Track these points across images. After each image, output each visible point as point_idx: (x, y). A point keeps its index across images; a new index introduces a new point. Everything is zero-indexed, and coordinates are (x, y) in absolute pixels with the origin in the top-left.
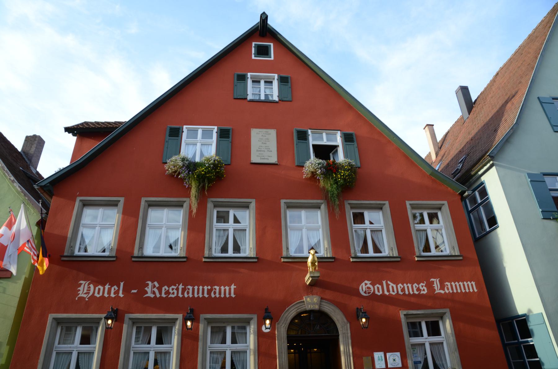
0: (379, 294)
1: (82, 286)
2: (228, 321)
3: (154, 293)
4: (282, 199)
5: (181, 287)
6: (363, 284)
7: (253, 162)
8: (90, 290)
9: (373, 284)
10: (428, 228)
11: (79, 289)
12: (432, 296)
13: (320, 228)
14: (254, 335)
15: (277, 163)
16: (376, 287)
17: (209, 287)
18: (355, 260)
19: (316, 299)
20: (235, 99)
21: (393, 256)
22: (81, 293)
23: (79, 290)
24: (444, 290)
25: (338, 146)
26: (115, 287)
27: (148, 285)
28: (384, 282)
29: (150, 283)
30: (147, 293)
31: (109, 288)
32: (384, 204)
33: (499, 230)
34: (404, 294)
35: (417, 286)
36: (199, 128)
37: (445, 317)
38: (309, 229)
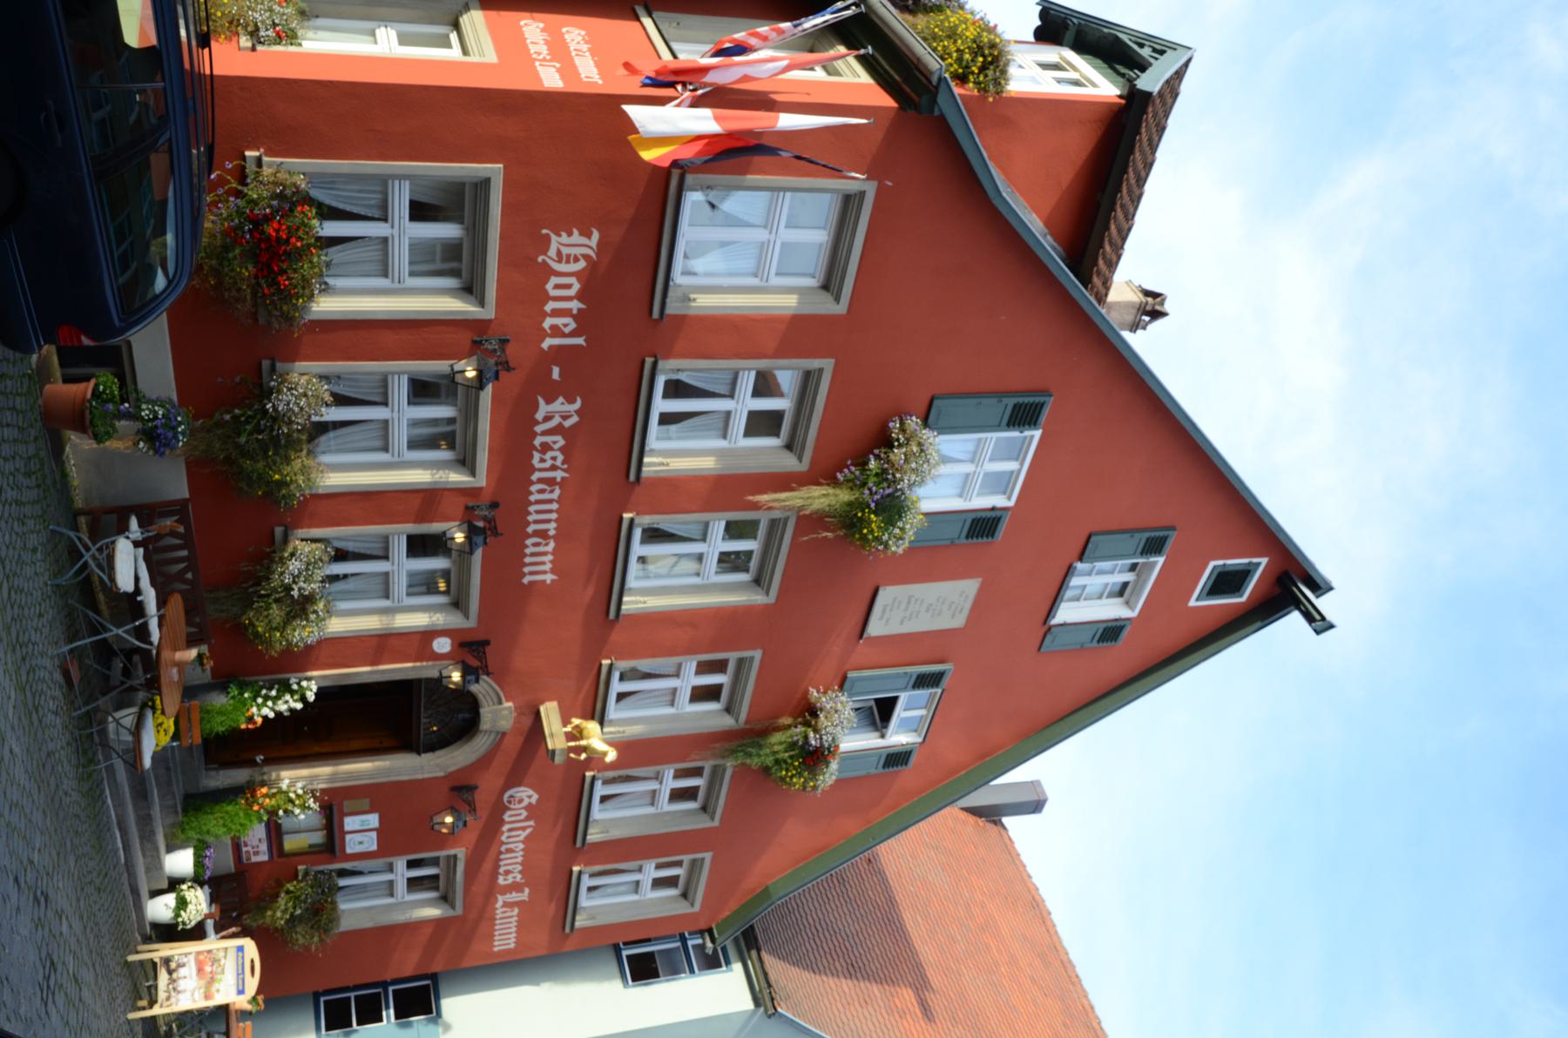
0: (549, 286)
1: (584, 240)
2: (477, 231)
3: (547, 418)
4: (764, 654)
5: (559, 475)
6: (531, 792)
7: (881, 593)
8: (568, 262)
9: (529, 807)
10: (738, 402)
11: (576, 232)
12: (492, 890)
13: (761, 280)
14: (430, 483)
15: (865, 636)
16: (573, 280)
17: (552, 533)
18: (588, 781)
19: (506, 723)
20: (1089, 537)
21: (646, 454)
22: (560, 240)
23: (570, 234)
24: (503, 906)
25: (883, 736)
26: (573, 325)
27: (571, 401)
28: (531, 823)
29: (578, 404)
30: (549, 401)
31: (571, 310)
32: (837, 299)
33: (617, 984)
34: (501, 853)
35: (556, 446)
36: (1022, 464)
37: (447, 907)
38: (763, 247)
